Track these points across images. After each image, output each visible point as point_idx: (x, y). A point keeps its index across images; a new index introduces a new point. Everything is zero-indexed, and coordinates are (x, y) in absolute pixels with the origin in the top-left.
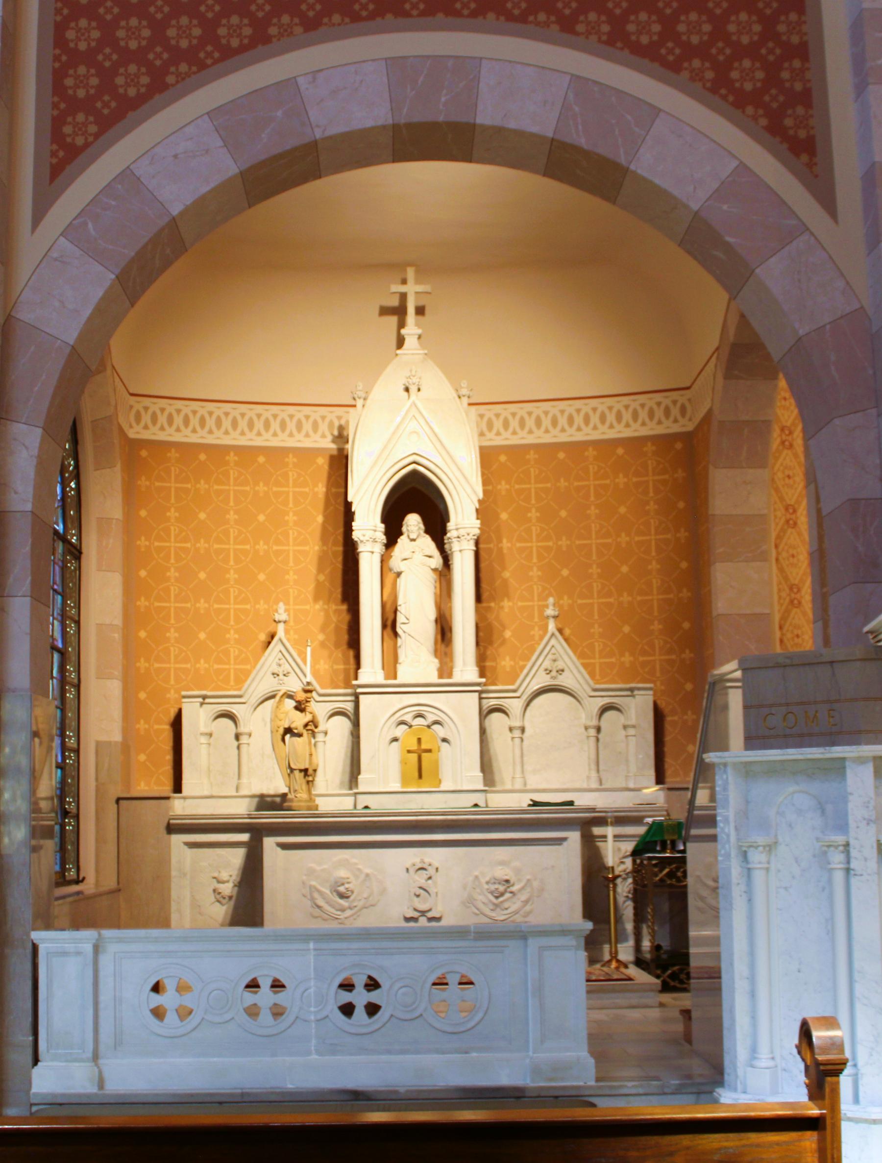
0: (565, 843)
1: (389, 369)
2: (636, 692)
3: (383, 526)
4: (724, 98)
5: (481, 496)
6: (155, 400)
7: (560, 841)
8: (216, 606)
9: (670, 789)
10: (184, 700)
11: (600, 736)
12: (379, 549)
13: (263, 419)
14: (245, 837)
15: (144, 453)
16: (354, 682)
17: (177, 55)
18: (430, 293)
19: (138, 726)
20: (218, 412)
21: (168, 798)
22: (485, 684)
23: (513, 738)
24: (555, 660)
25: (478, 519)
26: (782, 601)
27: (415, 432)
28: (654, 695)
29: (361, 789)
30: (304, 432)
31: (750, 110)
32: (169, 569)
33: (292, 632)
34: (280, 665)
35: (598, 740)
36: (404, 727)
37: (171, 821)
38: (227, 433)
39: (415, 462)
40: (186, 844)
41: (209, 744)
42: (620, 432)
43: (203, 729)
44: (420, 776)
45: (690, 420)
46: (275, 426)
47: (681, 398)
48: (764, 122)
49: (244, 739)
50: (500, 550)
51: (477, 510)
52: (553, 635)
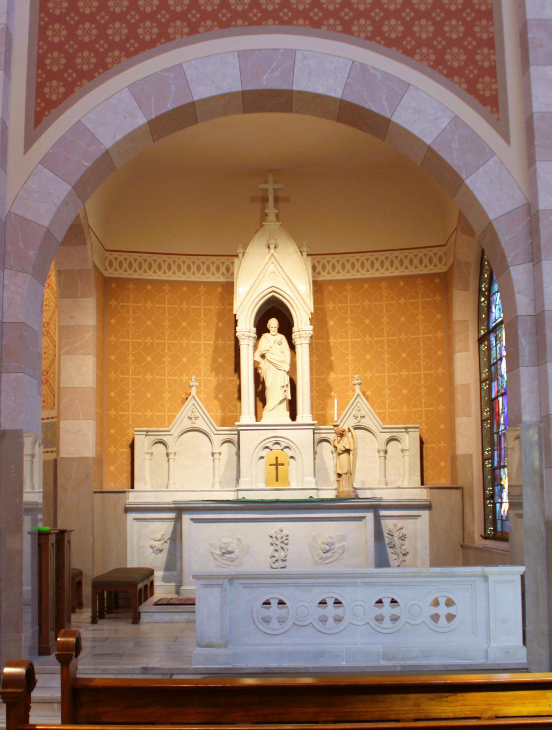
0: (364, 520)
1: (257, 235)
2: (409, 430)
3: (255, 329)
4: (440, 72)
5: (313, 311)
6: (111, 253)
7: (360, 519)
8: (121, 376)
9: (431, 488)
10: (136, 433)
11: (387, 456)
12: (252, 342)
13: (157, 263)
14: (172, 515)
15: (114, 285)
16: (236, 423)
17: (113, 46)
18: (283, 189)
19: (110, 449)
20: (149, 260)
21: (125, 492)
22: (318, 424)
23: (380, 456)
24: (359, 411)
25: (311, 325)
26: (54, 371)
27: (273, 272)
28: (421, 431)
29: (241, 487)
30: (143, 269)
31: (456, 79)
32: (128, 355)
33: (314, 392)
34: (193, 412)
35: (385, 458)
36: (268, 450)
37: (127, 506)
38: (135, 271)
39: (273, 291)
40: (192, 519)
41: (151, 459)
42: (402, 272)
43: (146, 451)
44: (277, 480)
45: (445, 265)
46: (145, 266)
47: (440, 252)
48: (465, 86)
49: (171, 456)
50: (329, 343)
51: (310, 319)
52: (358, 395)
